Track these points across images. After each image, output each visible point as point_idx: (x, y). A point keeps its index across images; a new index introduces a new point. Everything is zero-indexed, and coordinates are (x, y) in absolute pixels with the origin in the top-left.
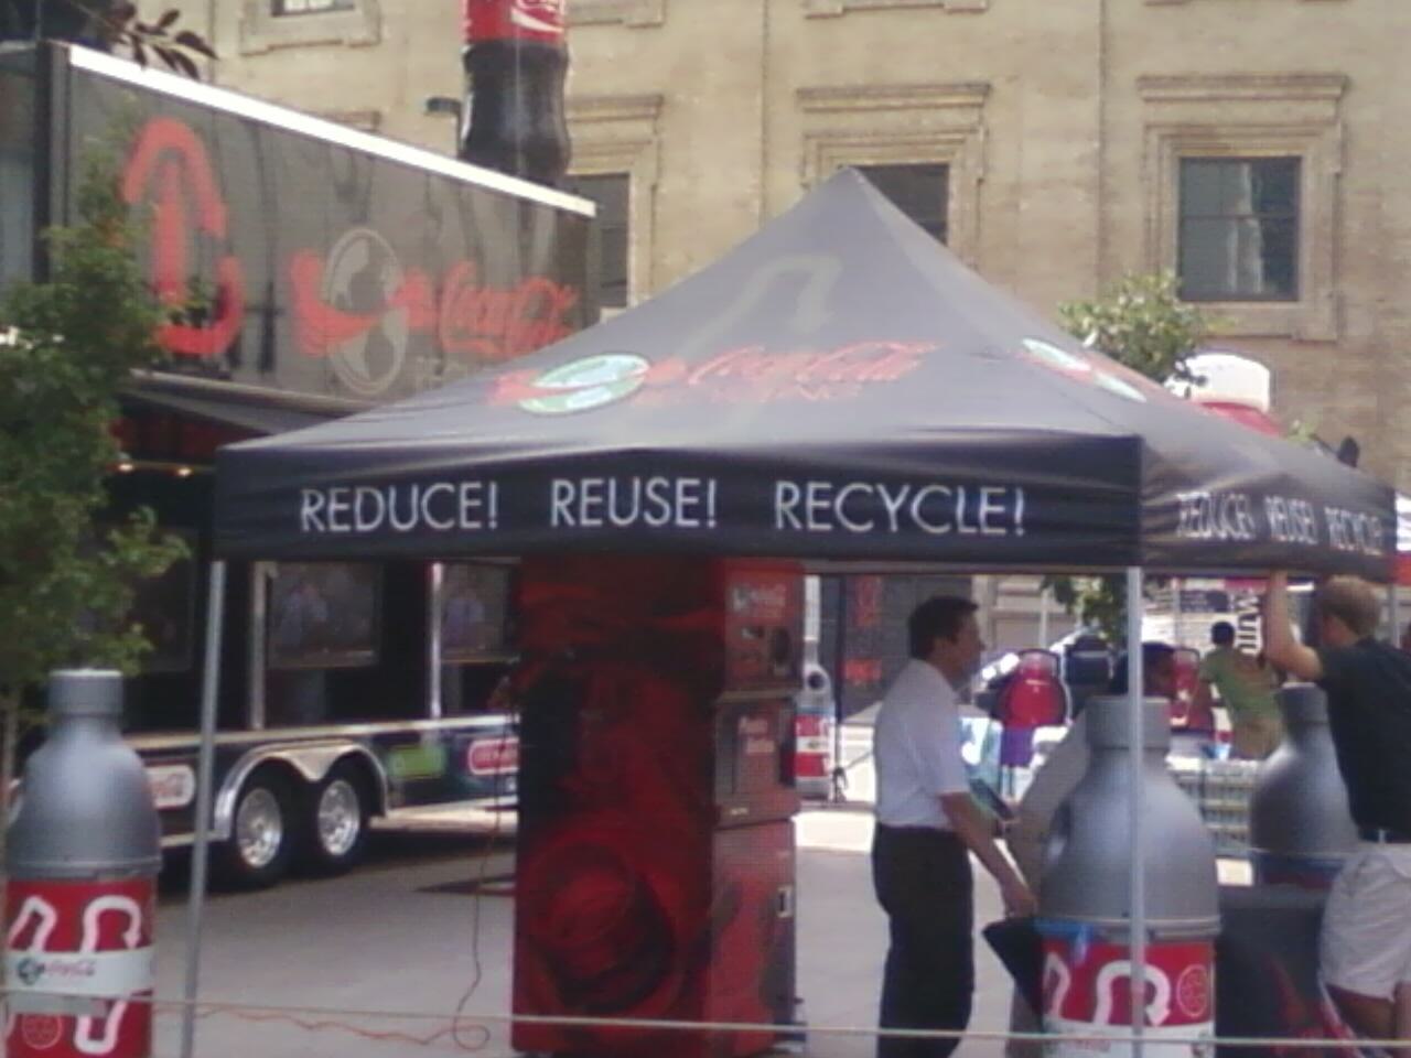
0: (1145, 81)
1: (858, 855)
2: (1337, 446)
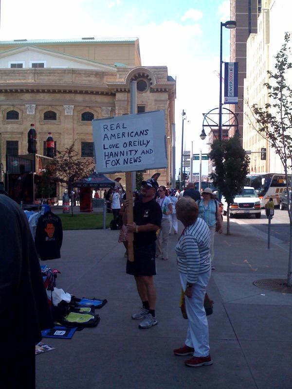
0: (78, 133)
1: (140, 64)
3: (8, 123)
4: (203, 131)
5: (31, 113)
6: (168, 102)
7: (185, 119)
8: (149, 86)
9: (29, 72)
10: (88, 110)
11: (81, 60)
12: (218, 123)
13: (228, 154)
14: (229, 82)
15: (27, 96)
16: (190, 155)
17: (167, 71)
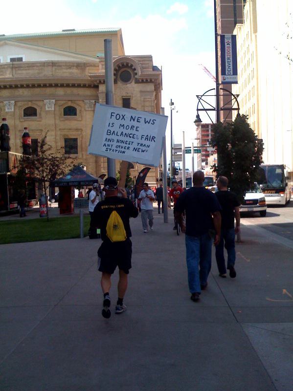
0: (60, 129)
1: (123, 52)
2: (105, 293)
4: (198, 116)
6: (154, 94)
7: (173, 109)
8: (134, 77)
9: (6, 67)
10: (70, 104)
11: (62, 52)
12: (214, 105)
13: (234, 142)
14: (226, 57)
16: (181, 148)
17: (152, 61)
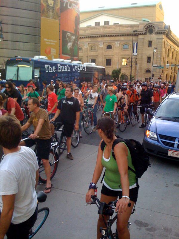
3: (92, 51)
5: (101, 47)
15: (100, 39)
